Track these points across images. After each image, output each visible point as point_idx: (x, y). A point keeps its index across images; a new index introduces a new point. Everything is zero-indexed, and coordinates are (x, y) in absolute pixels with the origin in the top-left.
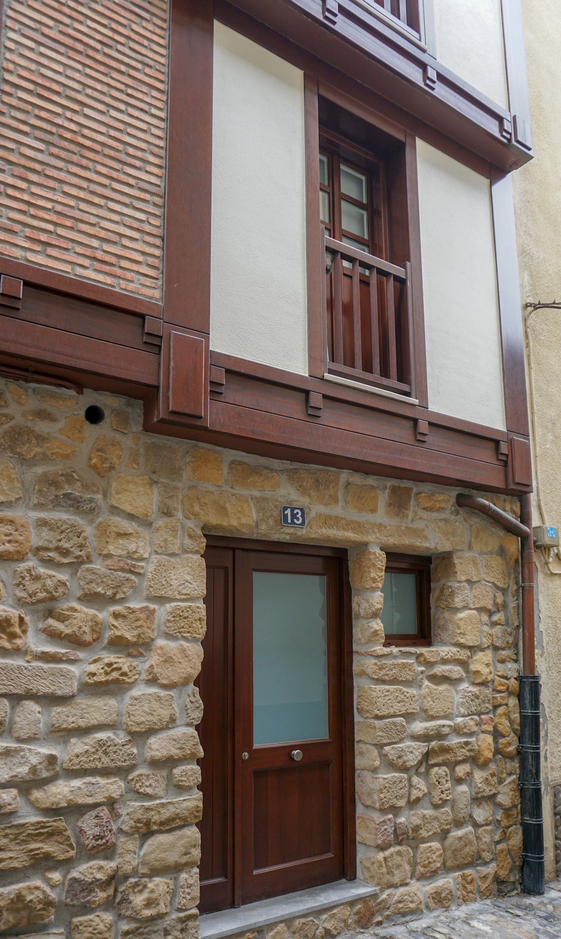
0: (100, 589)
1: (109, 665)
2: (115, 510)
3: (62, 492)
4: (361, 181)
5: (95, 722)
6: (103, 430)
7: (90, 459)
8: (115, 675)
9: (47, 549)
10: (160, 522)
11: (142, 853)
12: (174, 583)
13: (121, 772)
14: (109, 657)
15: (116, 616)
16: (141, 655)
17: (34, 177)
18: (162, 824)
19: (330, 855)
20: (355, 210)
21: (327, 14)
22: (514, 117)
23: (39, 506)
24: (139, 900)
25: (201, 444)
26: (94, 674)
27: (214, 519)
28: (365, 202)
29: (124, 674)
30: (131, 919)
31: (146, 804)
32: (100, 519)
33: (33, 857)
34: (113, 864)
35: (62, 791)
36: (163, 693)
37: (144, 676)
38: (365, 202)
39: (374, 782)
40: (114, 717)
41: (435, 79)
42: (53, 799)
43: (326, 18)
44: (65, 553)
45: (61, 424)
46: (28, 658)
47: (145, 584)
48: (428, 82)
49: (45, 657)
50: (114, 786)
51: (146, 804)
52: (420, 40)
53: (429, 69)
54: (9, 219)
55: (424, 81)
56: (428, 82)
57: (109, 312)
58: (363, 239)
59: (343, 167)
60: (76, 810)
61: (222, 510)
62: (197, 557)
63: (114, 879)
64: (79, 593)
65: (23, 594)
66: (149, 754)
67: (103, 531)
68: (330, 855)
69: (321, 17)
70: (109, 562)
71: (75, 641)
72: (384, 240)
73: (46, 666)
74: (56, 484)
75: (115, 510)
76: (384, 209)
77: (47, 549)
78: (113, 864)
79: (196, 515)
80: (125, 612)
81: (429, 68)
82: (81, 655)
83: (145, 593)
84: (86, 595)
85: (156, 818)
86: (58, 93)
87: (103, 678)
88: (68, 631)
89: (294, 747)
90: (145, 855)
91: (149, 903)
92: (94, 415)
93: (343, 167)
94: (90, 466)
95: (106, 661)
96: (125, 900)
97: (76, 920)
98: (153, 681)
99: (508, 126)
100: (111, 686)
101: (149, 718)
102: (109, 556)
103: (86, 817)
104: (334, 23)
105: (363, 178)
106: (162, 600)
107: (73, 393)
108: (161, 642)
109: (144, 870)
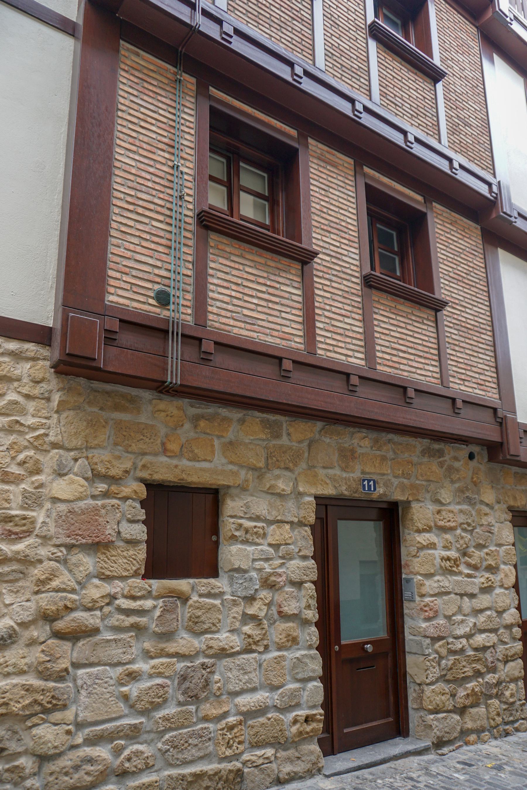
0: (481, 542)
1: (488, 578)
2: (482, 502)
3: (465, 496)
4: (264, 177)
5: (485, 606)
6: (473, 464)
7: (472, 478)
8: (490, 583)
9: (464, 524)
10: (496, 507)
11: (506, 671)
12: (504, 536)
13: (494, 631)
14: (487, 575)
15: (487, 554)
16: (496, 573)
17: (457, 348)
18: (511, 657)
19: (391, 719)
20: (251, 198)
21: (295, 77)
22: (499, 182)
23: (459, 503)
24: (507, 693)
25: (505, 465)
26: (483, 583)
27: (512, 503)
28: (267, 194)
29: (492, 583)
30: (505, 703)
31: (506, 647)
32: (477, 507)
33: (474, 671)
34: (497, 676)
35: (480, 639)
36: (506, 592)
37: (498, 584)
38: (267, 194)
39: (420, 666)
40: (491, 604)
41: (362, 111)
42: (478, 644)
43: (223, 39)
44: (469, 524)
45: (461, 463)
46: (463, 576)
47: (495, 538)
48: (356, 113)
49: (469, 576)
50: (493, 638)
51: (506, 647)
52: (440, 142)
53: (409, 134)
54: (453, 371)
55: (353, 112)
56: (356, 113)
57: (478, 407)
58: (266, 224)
59: (241, 164)
60: (485, 649)
61: (515, 498)
62: (508, 523)
63: (499, 683)
64: (474, 544)
65: (459, 546)
66: (504, 622)
67: (479, 512)
68: (391, 719)
69: (219, 39)
70: (482, 528)
71: (475, 568)
72: (281, 225)
73: (469, 580)
74: (463, 492)
75: (482, 502)
76: (282, 199)
77: (464, 524)
78: (497, 676)
79: (506, 501)
80: (490, 552)
81: (409, 134)
82: (477, 574)
83: (494, 543)
84: (477, 545)
85: (510, 654)
86: (457, 304)
87: (486, 585)
88: (473, 563)
89: (367, 643)
90: (508, 672)
91: (512, 695)
92: (471, 456)
93: (241, 164)
94: (472, 482)
95: (486, 576)
96: (502, 694)
97: (489, 702)
98: (502, 586)
99: (495, 189)
100: (487, 590)
101: (503, 604)
102: (482, 525)
103: (488, 652)
104: (230, 43)
105: (265, 175)
106: (500, 545)
107: (465, 447)
108: (502, 566)
109: (508, 680)
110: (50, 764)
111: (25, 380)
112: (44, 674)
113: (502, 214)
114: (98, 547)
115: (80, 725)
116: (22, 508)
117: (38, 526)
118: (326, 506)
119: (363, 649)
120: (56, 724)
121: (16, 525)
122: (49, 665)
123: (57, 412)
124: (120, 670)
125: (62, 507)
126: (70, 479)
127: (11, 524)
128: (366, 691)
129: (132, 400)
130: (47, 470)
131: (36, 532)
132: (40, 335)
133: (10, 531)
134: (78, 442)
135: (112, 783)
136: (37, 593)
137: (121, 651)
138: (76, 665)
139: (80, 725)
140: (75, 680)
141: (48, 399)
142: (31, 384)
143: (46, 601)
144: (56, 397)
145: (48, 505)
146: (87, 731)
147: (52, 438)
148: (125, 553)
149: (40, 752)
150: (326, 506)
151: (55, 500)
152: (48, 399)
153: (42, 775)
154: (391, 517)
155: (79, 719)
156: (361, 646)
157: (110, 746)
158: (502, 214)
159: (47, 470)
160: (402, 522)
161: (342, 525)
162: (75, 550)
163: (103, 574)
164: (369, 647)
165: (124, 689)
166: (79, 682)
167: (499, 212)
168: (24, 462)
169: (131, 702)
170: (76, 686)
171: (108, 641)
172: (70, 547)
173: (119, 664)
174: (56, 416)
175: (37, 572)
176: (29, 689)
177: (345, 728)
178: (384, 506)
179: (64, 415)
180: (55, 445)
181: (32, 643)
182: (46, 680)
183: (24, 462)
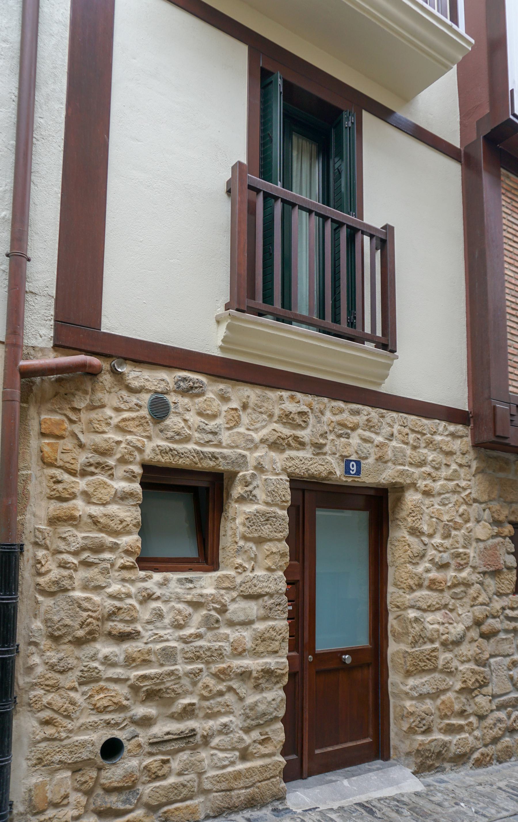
19: (369, 740)
110: (484, 722)
111: (458, 453)
112: (478, 662)
113: (511, 117)
114: (496, 573)
115: (494, 696)
116: (464, 547)
117: (471, 559)
118: (303, 491)
119: (341, 658)
120: (485, 695)
121: (462, 559)
122: (481, 656)
123: (474, 476)
124: (508, 659)
125: (481, 545)
126: (484, 524)
127: (460, 559)
128: (337, 708)
129: (507, 462)
130: (472, 519)
131: (470, 564)
132: (452, 415)
133: (459, 564)
134: (485, 498)
135: (508, 737)
136: (472, 606)
137: (508, 646)
138: (492, 656)
139: (494, 696)
140: (490, 666)
141: (469, 466)
142: (461, 456)
143: (479, 611)
144: (474, 465)
145: (474, 544)
146: (497, 700)
147: (473, 496)
148: (507, 577)
149: (480, 713)
150: (303, 491)
151: (478, 540)
152: (469, 466)
153: (480, 728)
154: (378, 506)
155: (494, 693)
156: (337, 655)
157: (505, 712)
158: (511, 117)
159: (472, 519)
160: (393, 512)
161: (319, 513)
162: (487, 576)
163: (499, 592)
164: (346, 657)
165: (511, 673)
166: (492, 667)
167: (509, 116)
168: (463, 514)
169: (514, 682)
170: (491, 670)
171: (503, 639)
172: (484, 573)
173: (508, 655)
174: (473, 478)
175: (472, 591)
176: (473, 672)
177: (316, 749)
178: (372, 493)
179: (477, 477)
180: (475, 501)
181: (473, 640)
182: (479, 666)
183: (463, 514)
